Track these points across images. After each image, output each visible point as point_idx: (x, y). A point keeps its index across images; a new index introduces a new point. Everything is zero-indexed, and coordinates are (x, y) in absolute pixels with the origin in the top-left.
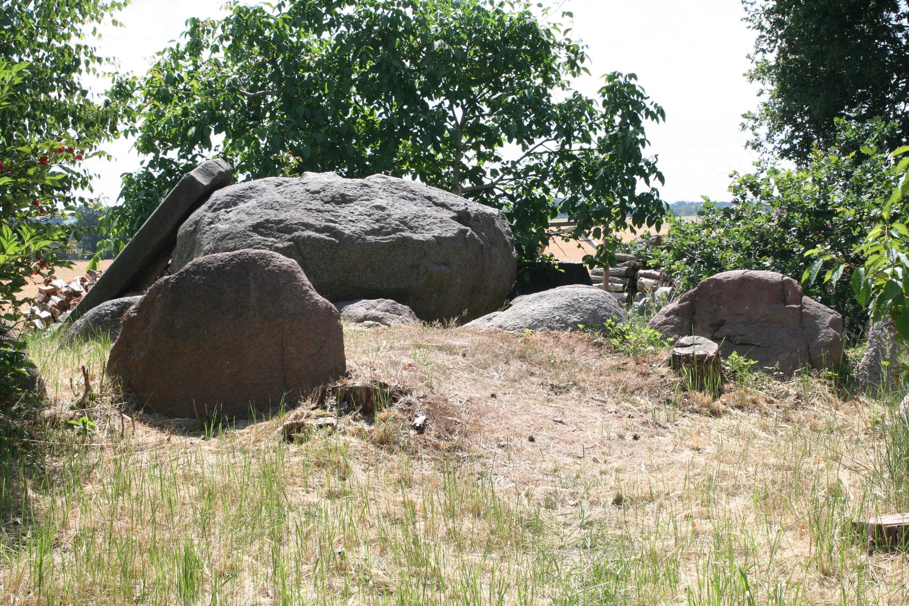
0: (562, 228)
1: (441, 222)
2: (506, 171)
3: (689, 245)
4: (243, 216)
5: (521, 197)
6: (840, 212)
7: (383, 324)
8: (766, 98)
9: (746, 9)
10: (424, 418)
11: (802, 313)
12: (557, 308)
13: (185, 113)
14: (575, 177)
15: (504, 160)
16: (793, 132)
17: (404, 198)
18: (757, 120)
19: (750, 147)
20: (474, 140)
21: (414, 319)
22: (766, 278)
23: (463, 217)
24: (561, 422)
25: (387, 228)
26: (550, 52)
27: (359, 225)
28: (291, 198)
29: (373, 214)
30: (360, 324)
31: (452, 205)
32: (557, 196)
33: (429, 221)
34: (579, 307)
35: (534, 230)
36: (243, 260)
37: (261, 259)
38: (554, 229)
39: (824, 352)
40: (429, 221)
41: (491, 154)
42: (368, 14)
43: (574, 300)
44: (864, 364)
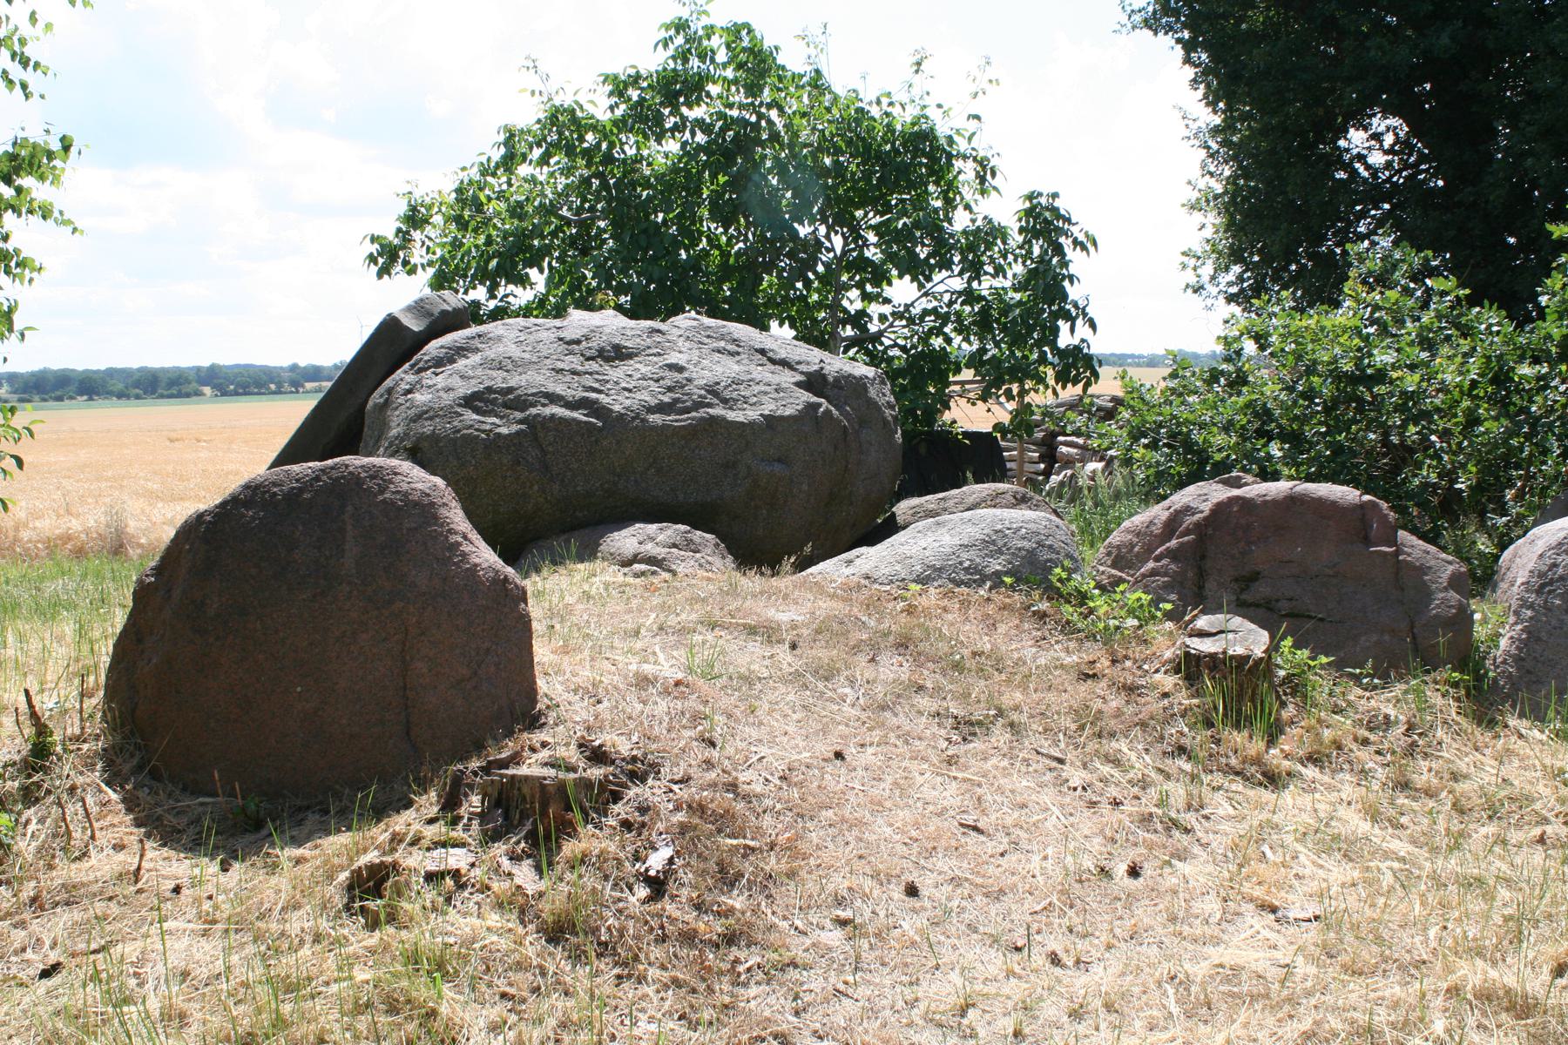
0: (967, 387)
1: (776, 390)
2: (897, 315)
3: (1155, 422)
4: (456, 382)
5: (916, 348)
6: (1398, 378)
7: (664, 570)
8: (1208, 232)
9: (1187, 126)
10: (665, 853)
11: (1398, 561)
12: (966, 546)
13: (489, 242)
14: (984, 323)
15: (896, 303)
16: (1244, 272)
17: (719, 352)
18: (1199, 258)
19: (1190, 291)
20: (857, 278)
21: (724, 558)
22: (1332, 498)
23: (814, 382)
24: (975, 829)
25: (684, 402)
26: (953, 165)
27: (638, 396)
28: (534, 350)
29: (663, 378)
30: (626, 570)
31: (799, 363)
32: (963, 347)
33: (757, 389)
34: (1005, 545)
35: (932, 390)
36: (338, 479)
37: (373, 477)
38: (957, 388)
39: (1444, 636)
40: (757, 389)
41: (879, 295)
42: (722, 116)
43: (997, 532)
44: (1506, 652)
